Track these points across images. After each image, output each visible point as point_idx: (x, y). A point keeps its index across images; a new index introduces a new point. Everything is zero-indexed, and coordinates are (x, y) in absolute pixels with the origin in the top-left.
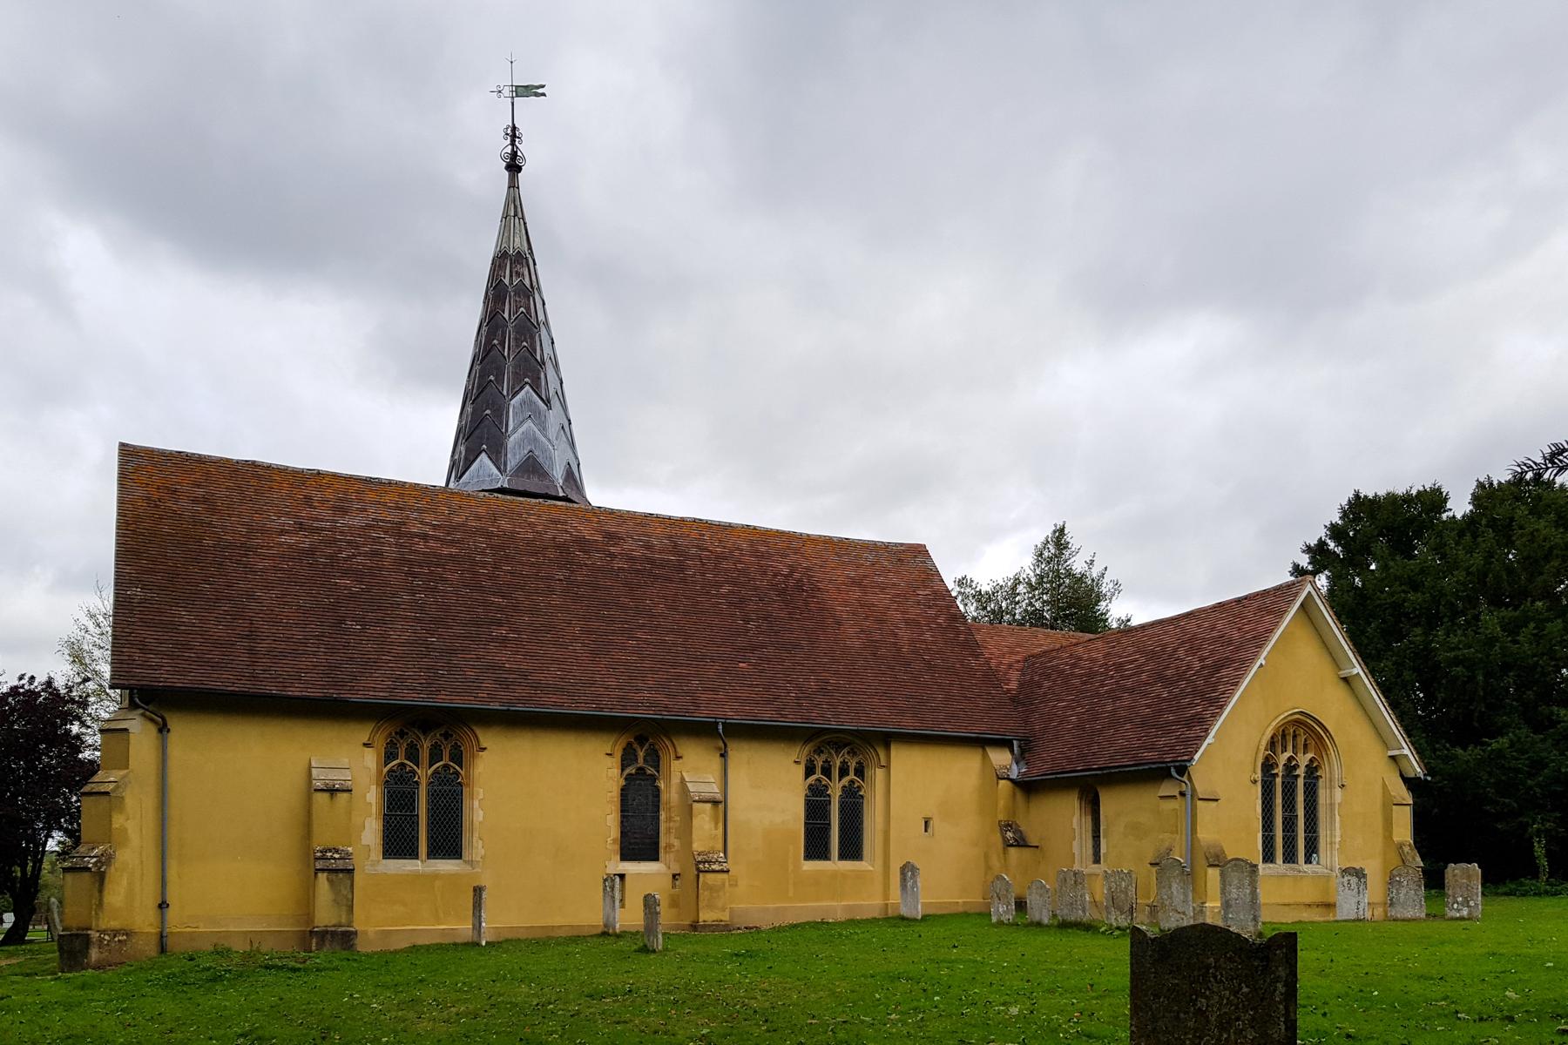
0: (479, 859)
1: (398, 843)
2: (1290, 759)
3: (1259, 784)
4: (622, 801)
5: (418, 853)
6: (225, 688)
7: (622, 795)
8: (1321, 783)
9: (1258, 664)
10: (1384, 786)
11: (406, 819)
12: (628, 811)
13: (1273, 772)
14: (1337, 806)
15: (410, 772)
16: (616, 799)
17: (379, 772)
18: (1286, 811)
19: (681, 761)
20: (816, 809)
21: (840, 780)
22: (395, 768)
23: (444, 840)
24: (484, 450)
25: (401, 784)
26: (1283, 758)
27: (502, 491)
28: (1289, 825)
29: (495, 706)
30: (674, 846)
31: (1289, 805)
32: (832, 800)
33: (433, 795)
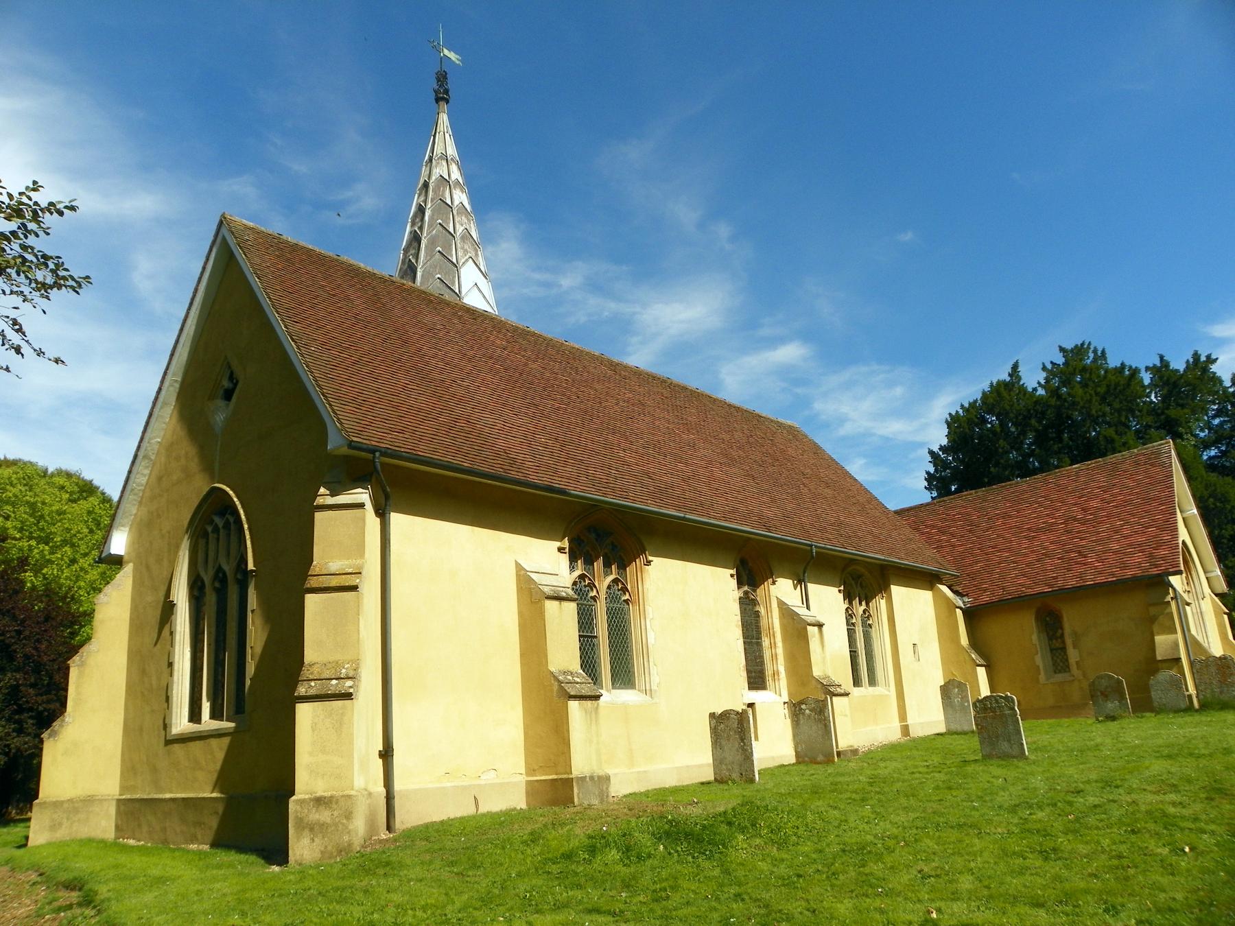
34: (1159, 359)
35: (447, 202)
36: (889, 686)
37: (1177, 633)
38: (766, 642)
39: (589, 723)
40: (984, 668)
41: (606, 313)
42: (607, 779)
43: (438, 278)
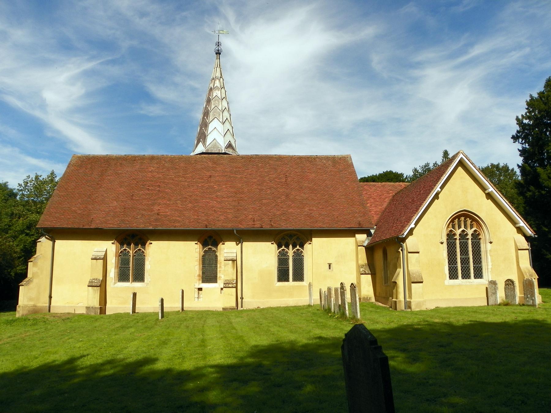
3: (445, 245)
6: (67, 227)
7: (203, 259)
8: (481, 241)
11: (126, 268)
12: (205, 264)
13: (455, 238)
22: (281, 251)
25: (125, 256)
26: (458, 232)
29: (151, 228)
30: (221, 277)
31: (464, 251)
37: (401, 268)
40: (370, 275)
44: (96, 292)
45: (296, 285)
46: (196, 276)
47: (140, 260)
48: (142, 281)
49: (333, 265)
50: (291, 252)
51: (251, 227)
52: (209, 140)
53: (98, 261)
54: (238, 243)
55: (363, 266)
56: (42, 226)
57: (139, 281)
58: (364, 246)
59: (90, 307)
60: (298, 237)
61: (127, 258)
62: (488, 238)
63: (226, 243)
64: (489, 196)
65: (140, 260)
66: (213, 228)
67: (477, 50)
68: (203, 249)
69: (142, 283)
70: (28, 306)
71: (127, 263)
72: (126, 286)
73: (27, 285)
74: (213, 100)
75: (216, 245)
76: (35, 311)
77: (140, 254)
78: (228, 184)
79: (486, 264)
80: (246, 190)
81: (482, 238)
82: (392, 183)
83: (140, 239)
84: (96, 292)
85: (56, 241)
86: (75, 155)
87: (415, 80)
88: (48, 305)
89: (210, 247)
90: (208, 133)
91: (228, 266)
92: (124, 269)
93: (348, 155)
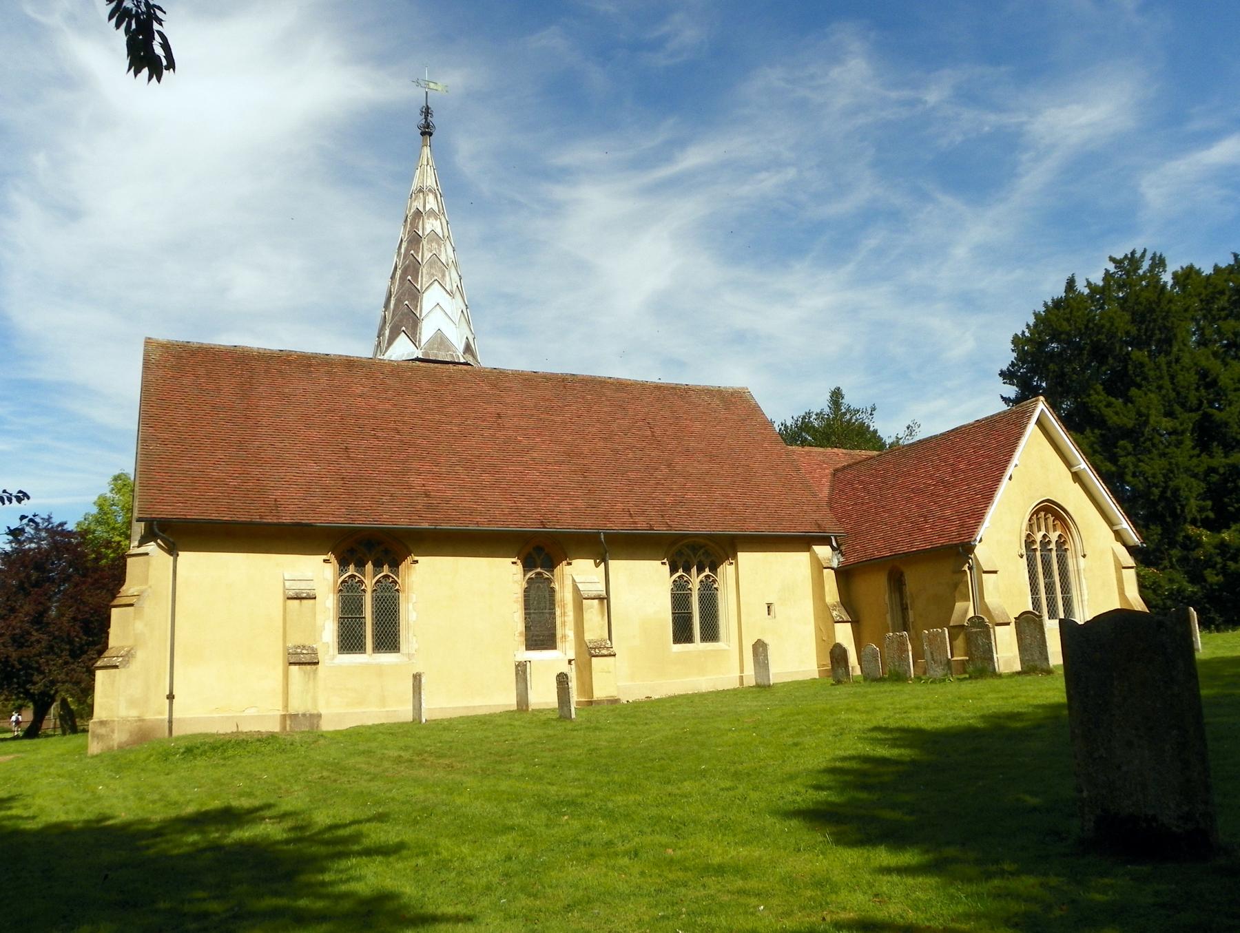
0: (414, 652)
1: (350, 641)
2: (1044, 536)
3: (1025, 557)
4: (526, 601)
5: (365, 648)
6: (221, 518)
7: (525, 596)
8: (1069, 553)
9: (1014, 465)
10: (1114, 553)
12: (530, 609)
14: (1082, 571)
15: (359, 582)
16: (520, 599)
17: (335, 582)
18: (1046, 577)
19: (570, 566)
20: (680, 601)
21: (698, 576)
23: (386, 638)
24: (403, 331)
26: (1038, 537)
27: (418, 359)
28: (1050, 588)
29: (425, 525)
31: (1048, 573)
32: (693, 593)
33: (376, 600)
34: (1233, 258)
35: (419, 233)
36: (729, 641)
37: (970, 601)
38: (558, 612)
39: (307, 680)
40: (849, 624)
41: (987, 129)
42: (319, 716)
43: (406, 305)
44: (309, 678)
45: (709, 648)
46: (516, 635)
47: (388, 600)
48: (394, 649)
49: (776, 606)
50: (695, 581)
51: (630, 528)
52: (427, 331)
53: (304, 602)
54: (598, 561)
55: (835, 606)
56: (154, 516)
57: (354, 651)
58: (832, 568)
59: (298, 714)
60: (706, 551)
61: (356, 596)
62: (1079, 548)
63: (575, 562)
64: (1077, 477)
65: (388, 600)
66: (558, 528)
67: (694, 158)
68: (525, 575)
69: (396, 654)
70: (129, 721)
71: (356, 608)
72: (361, 663)
73: (124, 667)
74: (426, 240)
75: (551, 565)
76: (143, 736)
77: (385, 585)
78: (545, 435)
79: (1079, 593)
80: (586, 450)
81: (1069, 548)
82: (821, 450)
83: (386, 552)
84: (309, 678)
85: (180, 553)
86: (149, 338)
87: (554, 209)
88: (166, 716)
89: (539, 570)
90: (423, 315)
91: (592, 611)
92: (350, 623)
93: (743, 388)
